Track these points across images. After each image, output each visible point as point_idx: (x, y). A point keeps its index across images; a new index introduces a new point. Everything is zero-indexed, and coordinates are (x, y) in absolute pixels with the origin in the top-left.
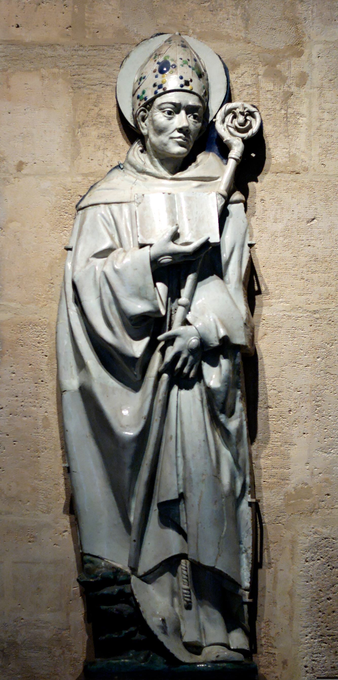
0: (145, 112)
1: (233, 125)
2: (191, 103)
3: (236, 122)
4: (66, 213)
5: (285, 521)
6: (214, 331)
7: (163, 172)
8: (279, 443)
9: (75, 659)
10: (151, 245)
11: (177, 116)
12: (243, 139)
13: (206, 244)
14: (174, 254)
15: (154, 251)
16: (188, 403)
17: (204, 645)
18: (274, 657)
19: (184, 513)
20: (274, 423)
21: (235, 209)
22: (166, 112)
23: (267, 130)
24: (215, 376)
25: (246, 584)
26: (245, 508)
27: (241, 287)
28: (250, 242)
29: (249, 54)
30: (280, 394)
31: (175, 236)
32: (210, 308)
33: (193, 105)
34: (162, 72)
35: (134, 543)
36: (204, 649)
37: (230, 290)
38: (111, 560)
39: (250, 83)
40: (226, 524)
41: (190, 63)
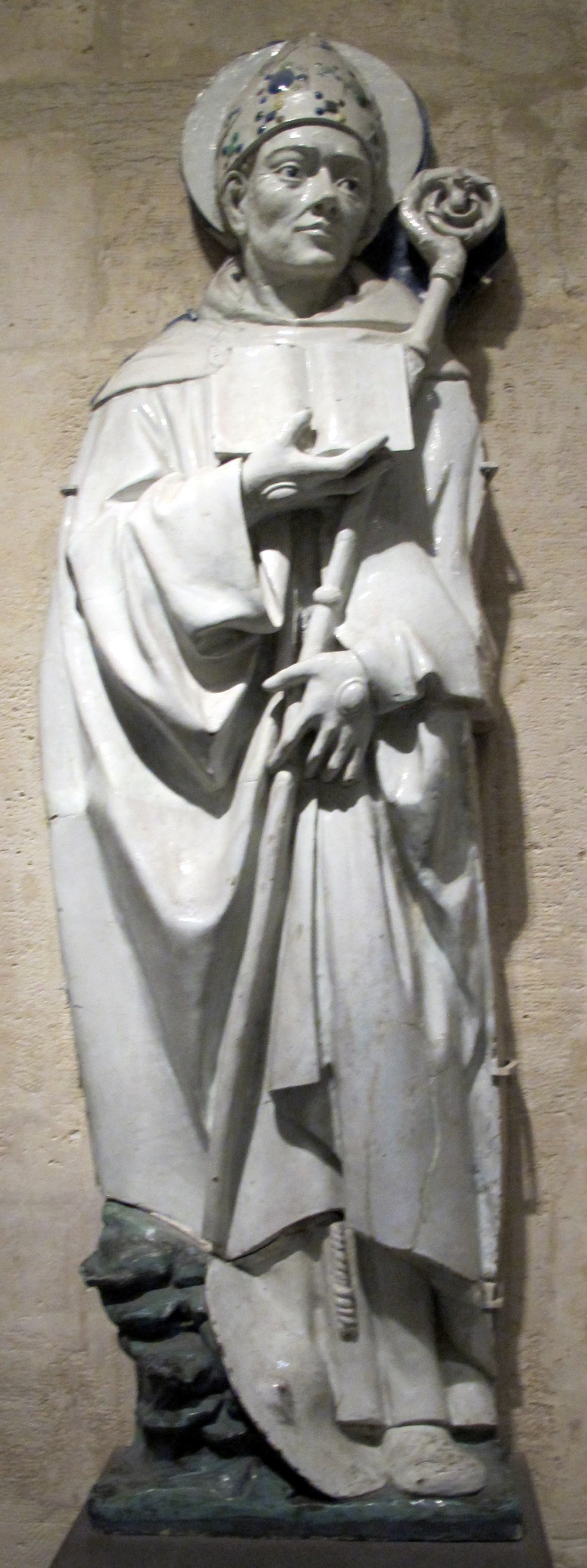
0: (239, 182)
1: (438, 211)
2: (340, 150)
3: (446, 207)
4: (78, 426)
5: (573, 1107)
6: (403, 663)
7: (280, 311)
8: (558, 929)
9: (101, 1419)
10: (245, 457)
11: (310, 179)
12: (462, 239)
13: (378, 455)
14: (300, 477)
15: (252, 470)
16: (341, 842)
17: (389, 1422)
18: (550, 1414)
19: (136, 601)
20: (547, 881)
21: (452, 394)
22: (285, 171)
23: (515, 236)
24: (407, 774)
25: (489, 1266)
26: (484, 1089)
27: (467, 565)
28: (484, 464)
29: (470, 85)
30: (558, 815)
31: (305, 436)
32: (392, 614)
33: (348, 154)
34: (274, 90)
35: (215, 1185)
36: (390, 1432)
37: (440, 571)
38: (165, 1215)
39: (472, 144)
40: (438, 1138)
41: (339, 73)
